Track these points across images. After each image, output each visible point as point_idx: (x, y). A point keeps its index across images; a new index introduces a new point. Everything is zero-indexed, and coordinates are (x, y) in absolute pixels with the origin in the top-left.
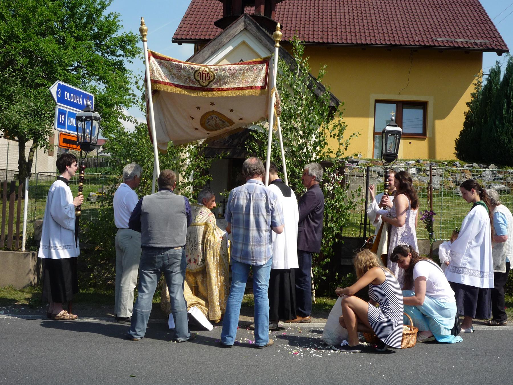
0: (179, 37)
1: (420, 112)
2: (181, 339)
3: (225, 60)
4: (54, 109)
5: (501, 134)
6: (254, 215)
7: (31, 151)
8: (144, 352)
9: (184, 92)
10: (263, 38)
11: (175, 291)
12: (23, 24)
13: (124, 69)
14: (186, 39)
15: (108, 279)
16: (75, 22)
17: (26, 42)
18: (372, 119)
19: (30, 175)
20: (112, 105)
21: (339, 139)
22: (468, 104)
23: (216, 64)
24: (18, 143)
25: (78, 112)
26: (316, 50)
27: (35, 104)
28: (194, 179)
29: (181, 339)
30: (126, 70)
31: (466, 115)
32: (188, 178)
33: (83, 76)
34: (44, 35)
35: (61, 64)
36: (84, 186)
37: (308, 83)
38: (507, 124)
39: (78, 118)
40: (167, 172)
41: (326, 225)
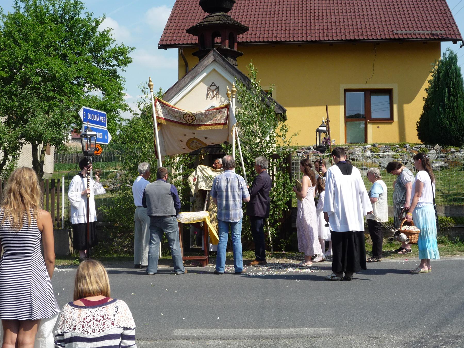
0: (164, 43)
1: (387, 98)
2: (179, 273)
3: (201, 83)
5: (443, 118)
6: (231, 191)
10: (227, 66)
13: (118, 77)
14: (171, 44)
17: (38, 63)
18: (343, 107)
22: (426, 90)
28: (183, 171)
30: (119, 78)
31: (425, 100)
32: (179, 171)
37: (260, 98)
38: (448, 110)
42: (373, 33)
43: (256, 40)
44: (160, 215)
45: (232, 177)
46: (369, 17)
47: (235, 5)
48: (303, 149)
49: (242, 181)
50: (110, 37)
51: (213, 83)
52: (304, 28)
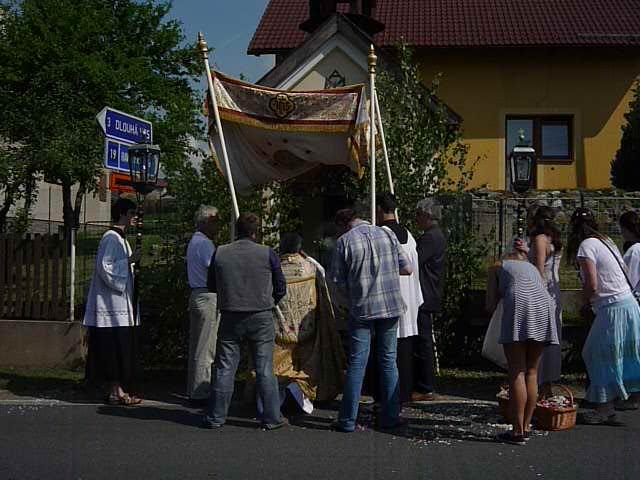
3: (314, 72)
4: (104, 142)
7: (79, 196)
8: (222, 441)
9: (256, 122)
11: (262, 365)
13: (190, 90)
15: (178, 353)
16: (126, 34)
17: (67, 62)
18: (504, 140)
19: (77, 225)
20: (177, 135)
21: (461, 168)
22: (626, 116)
23: (289, 91)
24: (61, 187)
25: (130, 144)
26: (428, 56)
27: (81, 138)
33: (139, 100)
34: (88, 51)
35: (111, 86)
36: (144, 236)
39: (131, 153)
40: (248, 214)
41: (451, 276)
51: (335, 71)
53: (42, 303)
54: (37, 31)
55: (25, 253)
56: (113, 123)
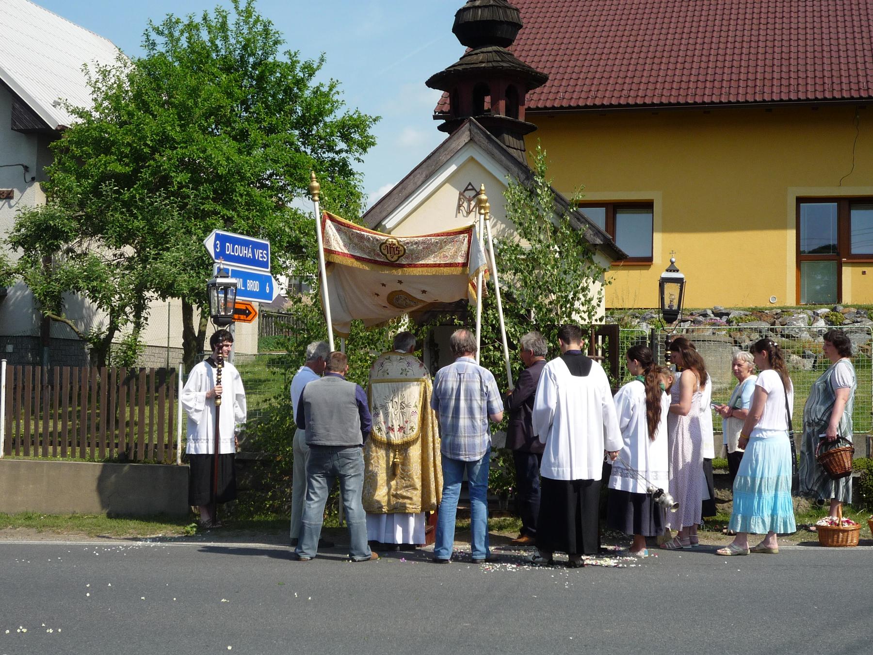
2: (358, 558)
3: (447, 185)
6: (466, 400)
10: (496, 152)
11: (350, 499)
12: (180, 118)
13: (351, 173)
17: (186, 147)
18: (791, 234)
29: (358, 558)
30: (353, 174)
42: (854, 86)
43: (672, 101)
44: (334, 444)
45: (470, 371)
46: (850, 53)
47: (520, 31)
48: (692, 314)
49: (489, 379)
50: (335, 98)
51: (470, 184)
52: (718, 77)
53: (147, 445)
54: (145, 107)
55: (129, 389)
56: (223, 247)
